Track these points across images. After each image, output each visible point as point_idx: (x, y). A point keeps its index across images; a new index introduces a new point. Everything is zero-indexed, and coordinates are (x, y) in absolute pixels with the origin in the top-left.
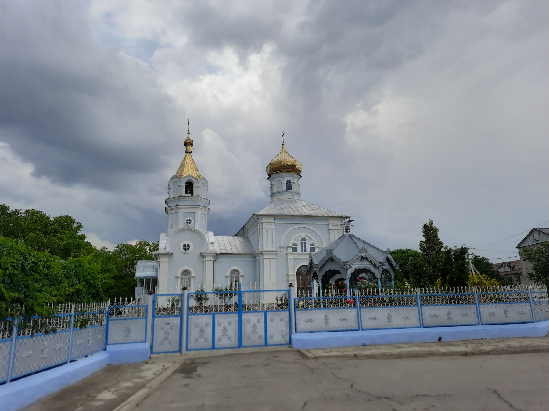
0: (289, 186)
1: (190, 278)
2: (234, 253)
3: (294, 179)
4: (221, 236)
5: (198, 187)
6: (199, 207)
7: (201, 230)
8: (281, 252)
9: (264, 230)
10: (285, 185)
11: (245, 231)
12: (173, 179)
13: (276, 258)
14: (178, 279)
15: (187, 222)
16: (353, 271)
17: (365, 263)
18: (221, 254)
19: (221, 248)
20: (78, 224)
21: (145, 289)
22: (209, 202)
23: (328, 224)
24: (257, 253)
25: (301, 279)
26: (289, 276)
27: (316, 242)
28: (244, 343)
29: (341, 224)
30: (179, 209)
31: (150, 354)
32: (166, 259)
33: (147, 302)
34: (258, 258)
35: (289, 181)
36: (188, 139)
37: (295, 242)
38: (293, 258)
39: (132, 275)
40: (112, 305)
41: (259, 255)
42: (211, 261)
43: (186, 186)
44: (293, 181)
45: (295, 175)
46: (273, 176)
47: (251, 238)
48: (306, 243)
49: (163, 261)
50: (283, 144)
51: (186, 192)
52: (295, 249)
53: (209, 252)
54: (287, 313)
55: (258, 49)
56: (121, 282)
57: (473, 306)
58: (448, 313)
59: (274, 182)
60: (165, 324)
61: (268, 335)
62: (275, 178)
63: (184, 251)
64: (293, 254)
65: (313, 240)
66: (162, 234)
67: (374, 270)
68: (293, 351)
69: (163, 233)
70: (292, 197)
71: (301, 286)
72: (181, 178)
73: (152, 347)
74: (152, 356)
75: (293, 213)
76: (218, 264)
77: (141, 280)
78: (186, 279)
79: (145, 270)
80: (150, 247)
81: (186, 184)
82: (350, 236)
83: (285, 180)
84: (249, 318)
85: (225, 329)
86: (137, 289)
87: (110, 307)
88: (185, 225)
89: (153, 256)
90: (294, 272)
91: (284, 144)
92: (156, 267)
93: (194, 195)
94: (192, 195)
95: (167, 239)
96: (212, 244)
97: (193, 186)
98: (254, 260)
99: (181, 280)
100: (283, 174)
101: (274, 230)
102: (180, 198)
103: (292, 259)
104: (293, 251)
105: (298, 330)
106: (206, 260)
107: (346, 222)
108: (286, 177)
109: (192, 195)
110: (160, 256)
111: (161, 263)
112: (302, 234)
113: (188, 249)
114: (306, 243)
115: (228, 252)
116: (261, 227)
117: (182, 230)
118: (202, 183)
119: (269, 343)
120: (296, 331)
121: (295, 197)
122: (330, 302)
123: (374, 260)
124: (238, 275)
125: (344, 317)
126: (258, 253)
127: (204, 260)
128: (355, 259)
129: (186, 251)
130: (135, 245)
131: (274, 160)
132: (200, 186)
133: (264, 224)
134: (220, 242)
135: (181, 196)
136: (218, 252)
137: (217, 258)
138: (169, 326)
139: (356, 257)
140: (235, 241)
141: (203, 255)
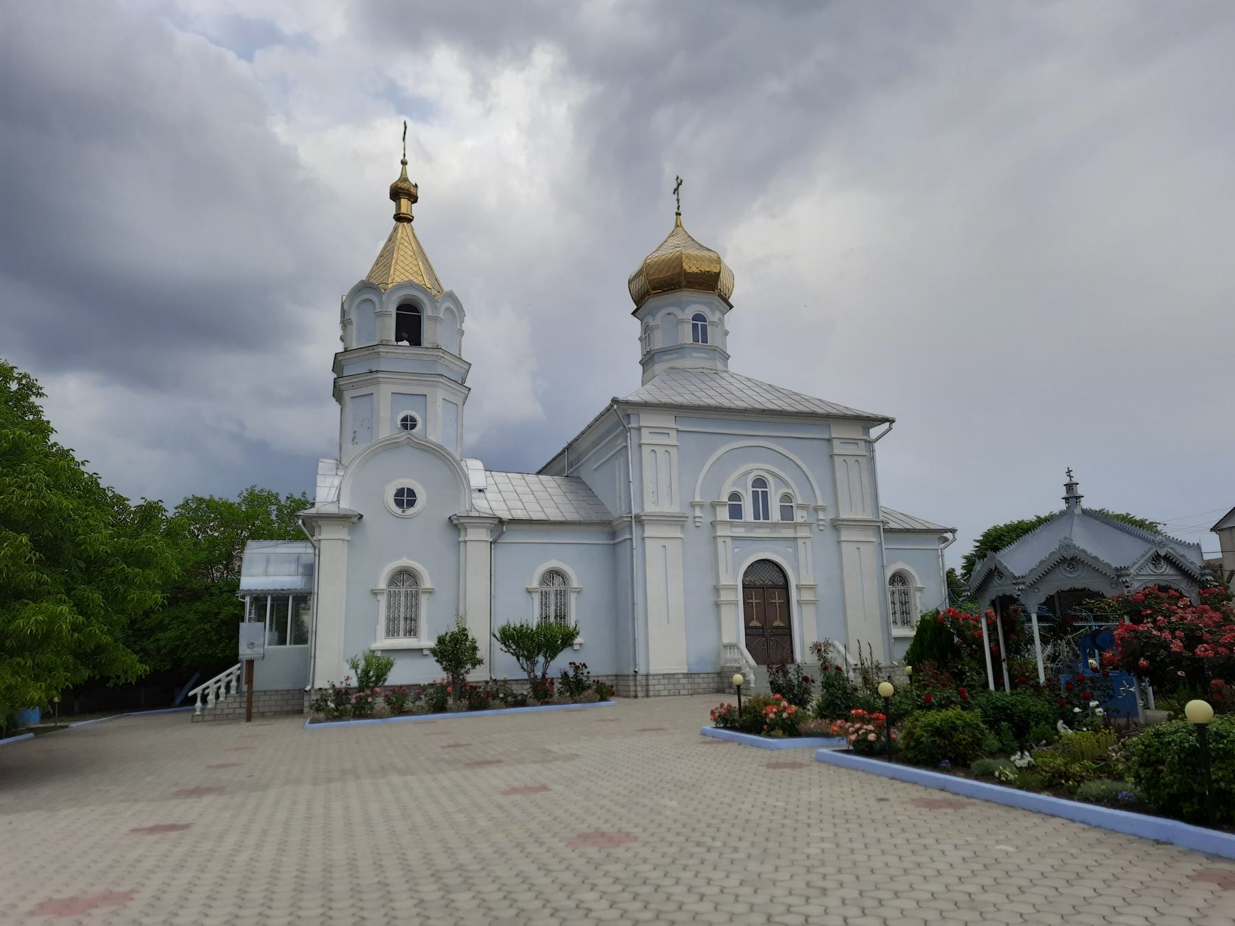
0: (700, 327)
1: (416, 595)
3: (712, 311)
5: (435, 319)
8: (697, 520)
9: (645, 450)
10: (688, 330)
12: (359, 291)
13: (682, 536)
14: (379, 597)
15: (402, 425)
18: (514, 522)
19: (511, 504)
20: (24, 382)
21: (271, 629)
23: (829, 440)
24: (625, 519)
25: (754, 601)
26: (722, 592)
27: (796, 490)
29: (866, 441)
30: (378, 383)
32: (342, 533)
34: (628, 536)
35: (698, 317)
36: (404, 179)
37: (735, 489)
38: (731, 537)
39: (226, 588)
41: (631, 527)
42: (485, 543)
44: (712, 317)
46: (652, 302)
49: (331, 541)
50: (678, 214)
52: (736, 512)
55: (522, 59)
56: (194, 607)
59: (657, 321)
62: (659, 309)
63: (398, 511)
64: (732, 525)
65: (787, 485)
71: (754, 623)
76: (502, 552)
77: (259, 599)
78: (403, 599)
79: (271, 569)
80: (279, 510)
83: (689, 313)
86: (244, 626)
89: (300, 522)
90: (736, 580)
96: (481, 494)
97: (420, 316)
98: (612, 542)
99: (389, 600)
100: (685, 295)
102: (381, 349)
103: (729, 541)
106: (466, 539)
108: (693, 304)
110: (320, 522)
111: (324, 546)
112: (757, 467)
113: (411, 503)
115: (535, 517)
116: (635, 441)
117: (391, 446)
118: (445, 309)
121: (718, 364)
124: (562, 587)
126: (629, 519)
127: (461, 539)
129: (403, 511)
130: (238, 500)
133: (644, 432)
136: (505, 515)
141: (456, 525)
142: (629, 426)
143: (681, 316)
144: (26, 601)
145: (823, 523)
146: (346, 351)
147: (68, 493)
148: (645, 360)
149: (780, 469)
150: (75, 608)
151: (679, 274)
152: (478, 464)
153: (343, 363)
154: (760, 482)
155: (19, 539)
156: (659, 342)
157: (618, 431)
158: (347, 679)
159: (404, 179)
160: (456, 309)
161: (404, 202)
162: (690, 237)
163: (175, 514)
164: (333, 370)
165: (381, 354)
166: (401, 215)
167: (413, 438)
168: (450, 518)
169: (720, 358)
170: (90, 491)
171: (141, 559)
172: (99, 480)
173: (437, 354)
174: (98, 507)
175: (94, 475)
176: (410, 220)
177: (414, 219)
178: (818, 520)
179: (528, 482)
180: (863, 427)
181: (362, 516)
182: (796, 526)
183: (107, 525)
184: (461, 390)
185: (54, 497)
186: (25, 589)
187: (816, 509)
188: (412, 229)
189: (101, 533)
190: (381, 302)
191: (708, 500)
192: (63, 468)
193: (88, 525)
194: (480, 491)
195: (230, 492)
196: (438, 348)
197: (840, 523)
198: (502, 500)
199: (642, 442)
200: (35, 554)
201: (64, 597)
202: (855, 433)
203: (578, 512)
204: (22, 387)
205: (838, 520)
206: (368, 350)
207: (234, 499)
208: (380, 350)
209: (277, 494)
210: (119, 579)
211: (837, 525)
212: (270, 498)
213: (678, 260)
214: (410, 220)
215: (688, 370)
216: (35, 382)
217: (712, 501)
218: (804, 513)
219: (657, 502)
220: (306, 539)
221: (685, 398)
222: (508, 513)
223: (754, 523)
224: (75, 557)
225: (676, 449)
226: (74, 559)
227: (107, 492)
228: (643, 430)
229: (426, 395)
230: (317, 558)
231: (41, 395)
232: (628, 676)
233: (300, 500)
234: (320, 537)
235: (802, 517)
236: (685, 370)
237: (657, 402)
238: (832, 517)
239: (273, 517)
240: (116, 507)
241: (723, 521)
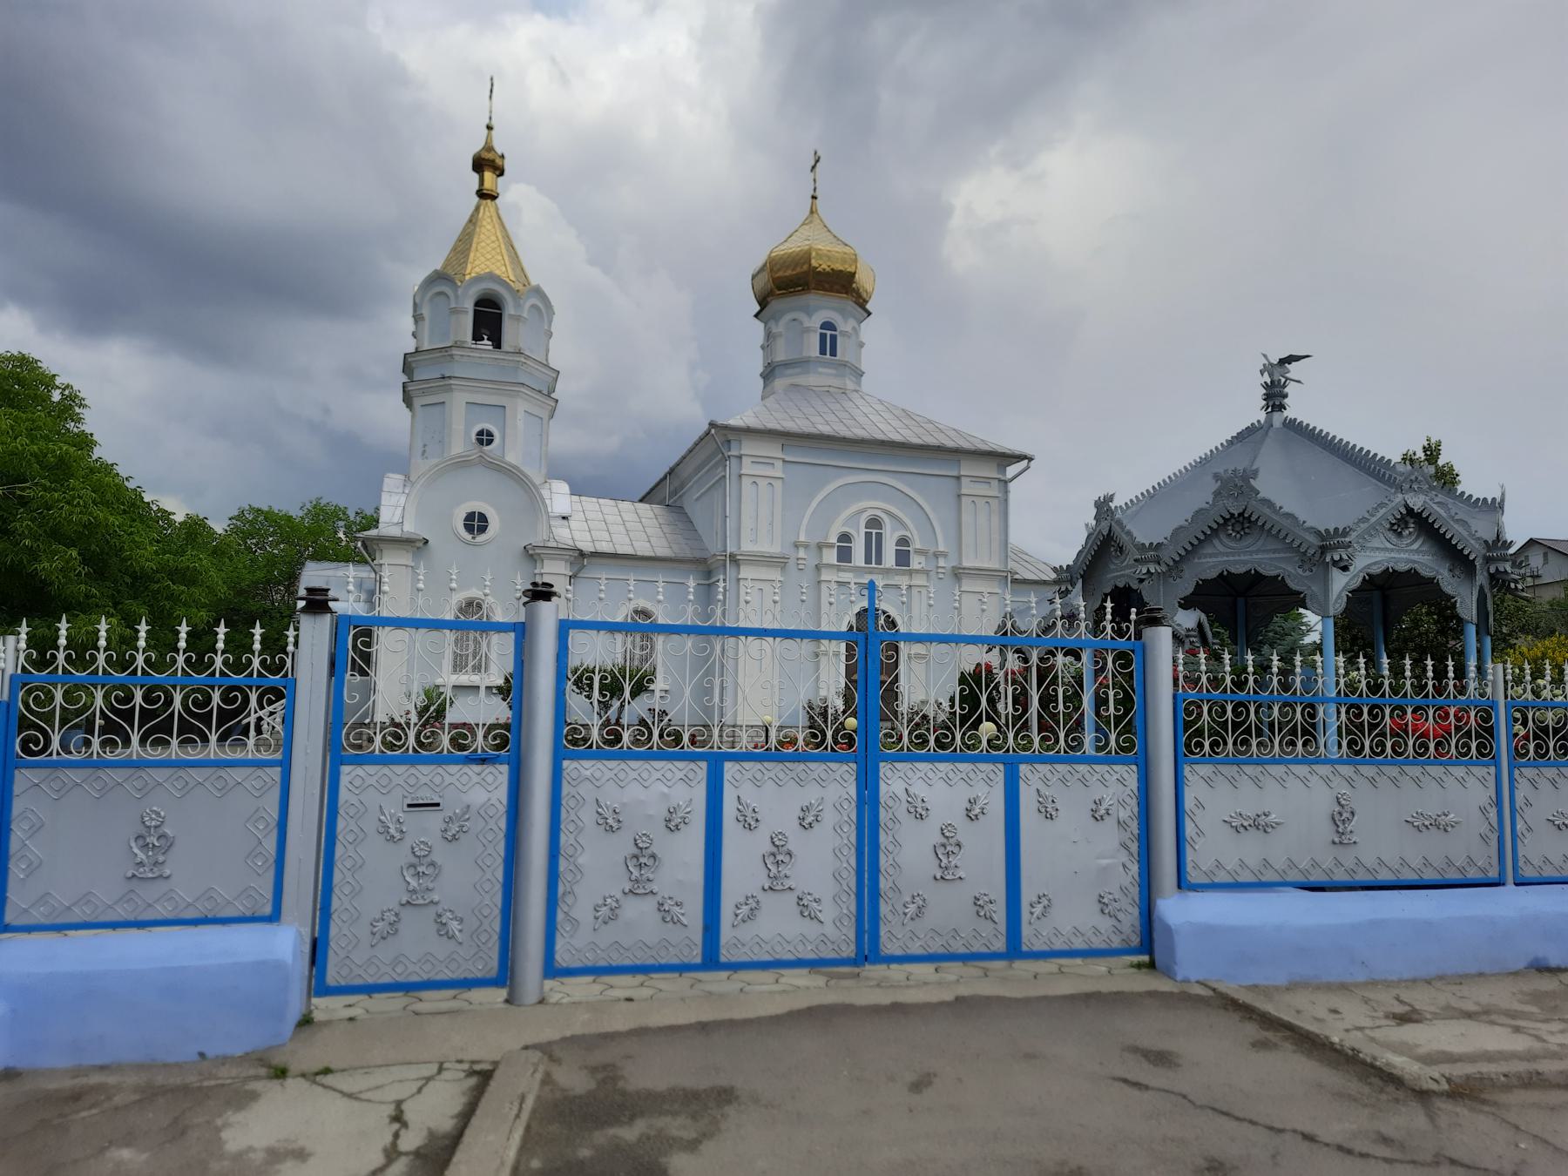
0: (829, 345)
2: (639, 553)
4: (594, 500)
5: (518, 318)
6: (522, 390)
7: (527, 470)
9: (746, 481)
11: (672, 488)
12: (433, 281)
16: (1357, 583)
17: (1415, 546)
18: (596, 555)
20: (67, 392)
22: (554, 376)
23: (958, 478)
24: (719, 558)
28: (893, 939)
29: (1000, 480)
31: (309, 996)
32: (404, 558)
33: (289, 662)
36: (489, 148)
40: (43, 662)
41: (725, 566)
43: (476, 313)
44: (844, 325)
45: (850, 305)
46: (775, 305)
47: (696, 510)
48: (881, 534)
50: (814, 197)
51: (477, 337)
52: (845, 554)
53: (554, 545)
54: (1130, 774)
57: (1479, 771)
58: (1337, 809)
59: (779, 328)
60: (410, 806)
61: (1027, 895)
63: (468, 537)
64: (839, 569)
66: (391, 475)
67: (1449, 582)
68: (1183, 999)
69: (393, 473)
70: (836, 382)
72: (462, 282)
73: (317, 951)
74: (325, 1007)
75: (843, 431)
81: (477, 304)
82: (1293, 426)
83: (816, 321)
84: (919, 789)
85: (779, 853)
87: (27, 678)
88: (474, 451)
89: (359, 544)
91: (816, 198)
92: (368, 585)
93: (506, 346)
94: (497, 344)
95: (407, 491)
96: (565, 522)
97: (501, 314)
98: (707, 582)
100: (813, 298)
101: (778, 484)
102: (455, 352)
103: (834, 586)
104: (838, 561)
105: (1193, 876)
106: (542, 571)
107: (1271, 364)
108: (822, 309)
109: (497, 344)
111: (386, 573)
112: (872, 505)
113: (482, 529)
114: (881, 534)
117: (462, 464)
119: (1031, 936)
120: (1182, 883)
121: (848, 382)
122: (1362, 724)
123: (1460, 529)
125: (1432, 811)
126: (723, 558)
127: (536, 571)
128: (1373, 520)
129: (474, 538)
130: (301, 514)
131: (782, 247)
132: (525, 315)
134: (590, 515)
135: (458, 345)
136: (587, 547)
137: (583, 566)
138: (433, 820)
139: (1382, 511)
140: (641, 515)
142: (729, 453)
143: (807, 324)
144: (76, 612)
145: (943, 571)
146: (417, 351)
147: (113, 508)
148: (766, 372)
149: (898, 509)
150: (123, 621)
151: (806, 273)
152: (562, 487)
153: (414, 365)
154: (874, 523)
155: (69, 553)
156: (780, 356)
157: (717, 459)
158: (407, 714)
159: (489, 148)
160: (544, 307)
161: (488, 175)
162: (825, 226)
163: (229, 526)
164: (403, 371)
165: (455, 357)
166: (485, 192)
167: (486, 457)
168: (525, 548)
169: (851, 374)
170: (133, 505)
171: (188, 577)
172: (143, 494)
173: (518, 359)
174: (142, 522)
175: (138, 489)
176: (494, 198)
177: (500, 197)
178: (938, 567)
179: (621, 510)
180: (998, 465)
181: (426, 542)
182: (911, 573)
183: (153, 541)
184: (547, 402)
185: (100, 513)
186: (73, 601)
187: (936, 555)
188: (497, 209)
189: (146, 549)
190: (457, 297)
191: (814, 541)
192: (108, 485)
193: (134, 541)
194: (564, 518)
195: (291, 502)
196: (520, 353)
197: (961, 571)
198: (587, 529)
199: (742, 472)
200: (84, 568)
201: (112, 610)
202: (989, 470)
203: (671, 547)
204: (64, 398)
205: (961, 568)
206: (440, 352)
207: (296, 513)
208: (454, 352)
209: (346, 508)
210: (165, 595)
211: (958, 574)
212: (337, 514)
213: (805, 257)
214: (494, 198)
215: (814, 388)
216: (78, 394)
217: (818, 541)
218: (922, 559)
219: (755, 541)
220: (366, 562)
221: (797, 424)
222: (591, 544)
223: (865, 568)
224: (121, 572)
225: (780, 481)
226: (120, 574)
227: (151, 505)
228: (744, 458)
229: (504, 407)
230: (378, 584)
231: (85, 406)
232: (1343, 866)
233: (372, 516)
234: (381, 562)
235: (920, 563)
236: (808, 388)
237: (763, 427)
238: (954, 564)
239: (341, 535)
240: (160, 522)
241: (828, 565)
